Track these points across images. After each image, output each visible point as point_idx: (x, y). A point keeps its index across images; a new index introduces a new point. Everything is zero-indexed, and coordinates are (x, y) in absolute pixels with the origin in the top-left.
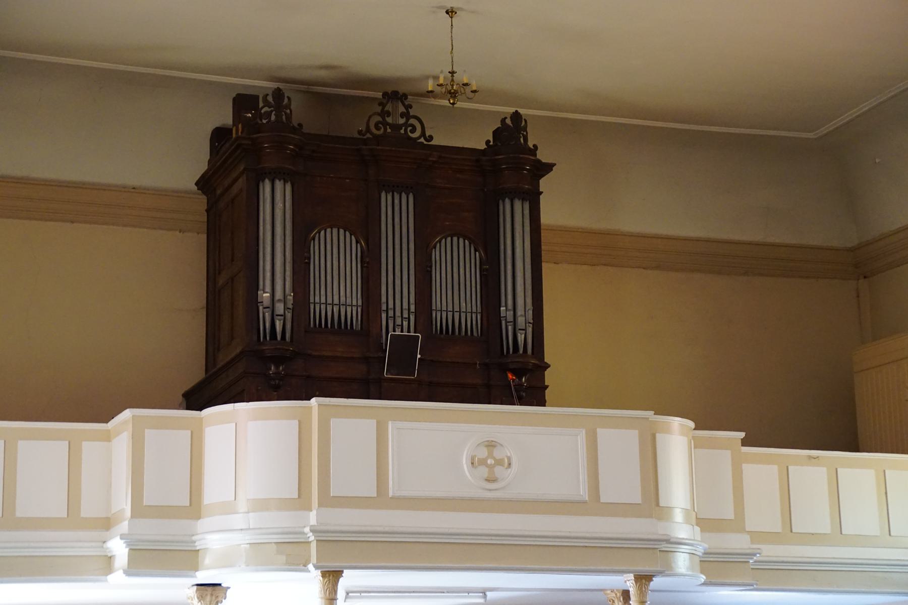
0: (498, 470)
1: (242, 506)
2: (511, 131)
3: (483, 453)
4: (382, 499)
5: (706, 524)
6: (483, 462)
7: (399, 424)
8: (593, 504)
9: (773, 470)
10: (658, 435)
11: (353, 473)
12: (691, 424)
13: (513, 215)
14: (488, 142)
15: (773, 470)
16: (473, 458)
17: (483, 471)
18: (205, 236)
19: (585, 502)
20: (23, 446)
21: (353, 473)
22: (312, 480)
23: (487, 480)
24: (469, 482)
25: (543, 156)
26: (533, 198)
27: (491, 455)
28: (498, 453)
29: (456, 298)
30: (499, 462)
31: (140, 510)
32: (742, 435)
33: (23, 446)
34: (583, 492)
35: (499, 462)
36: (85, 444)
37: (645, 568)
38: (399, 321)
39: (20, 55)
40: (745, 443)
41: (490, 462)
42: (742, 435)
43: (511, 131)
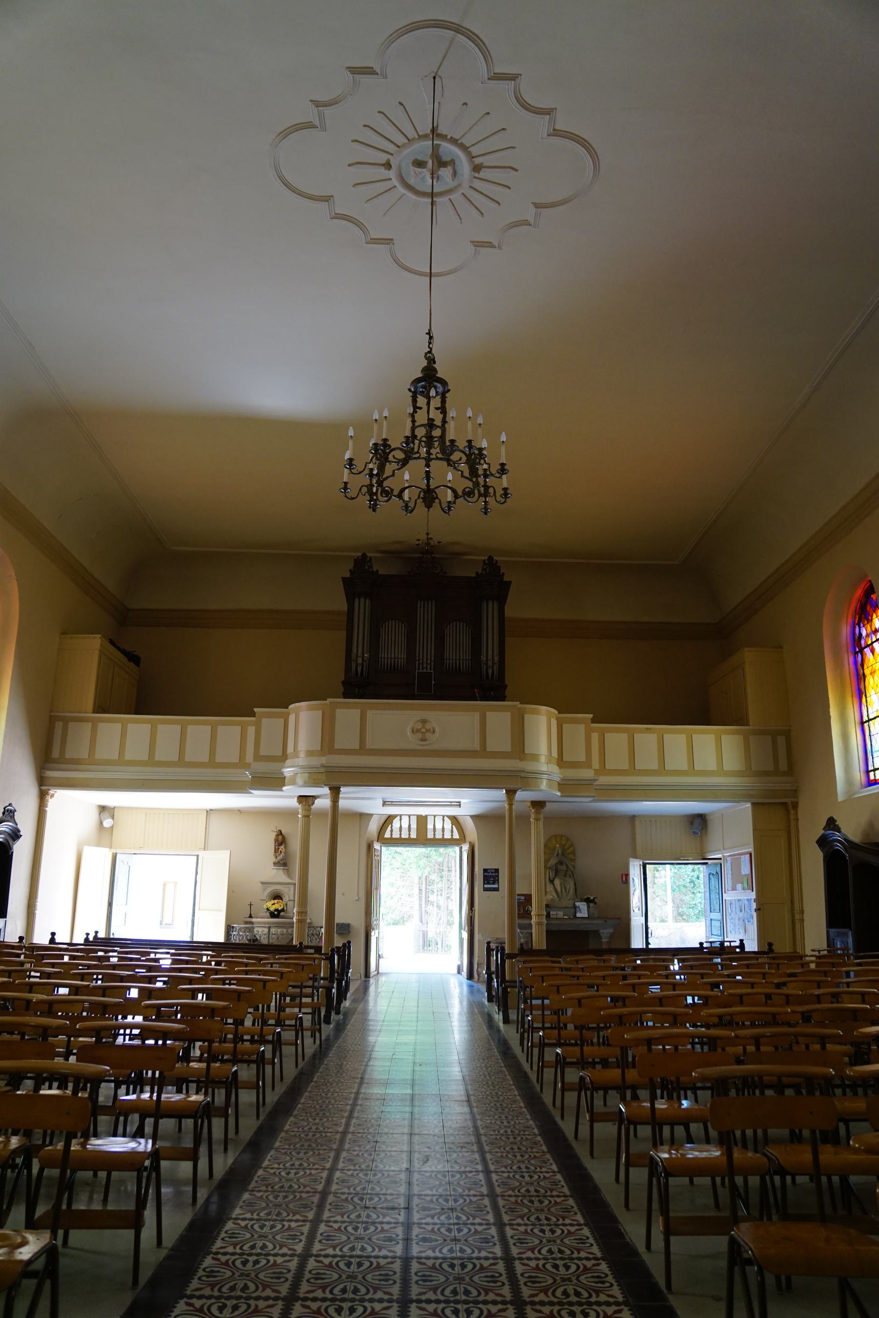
0: (428, 735)
1: (302, 755)
2: (491, 565)
3: (419, 726)
4: (362, 750)
5: (561, 762)
6: (418, 731)
7: (374, 712)
8: (483, 752)
9: (625, 736)
10: (526, 716)
11: (346, 737)
12: (556, 712)
13: (490, 609)
14: (477, 573)
15: (625, 736)
16: (413, 728)
17: (420, 735)
18: (345, 632)
19: (477, 751)
20: (220, 729)
21: (346, 737)
22: (327, 741)
23: (422, 740)
24: (412, 742)
25: (506, 579)
26: (502, 600)
27: (423, 727)
28: (428, 726)
29: (457, 652)
30: (428, 731)
31: (258, 757)
32: (591, 716)
33: (220, 729)
34: (477, 746)
35: (428, 731)
36: (219, 727)
37: (511, 786)
38: (425, 665)
39: (253, 551)
40: (593, 721)
41: (423, 730)
42: (591, 716)
43: (491, 565)
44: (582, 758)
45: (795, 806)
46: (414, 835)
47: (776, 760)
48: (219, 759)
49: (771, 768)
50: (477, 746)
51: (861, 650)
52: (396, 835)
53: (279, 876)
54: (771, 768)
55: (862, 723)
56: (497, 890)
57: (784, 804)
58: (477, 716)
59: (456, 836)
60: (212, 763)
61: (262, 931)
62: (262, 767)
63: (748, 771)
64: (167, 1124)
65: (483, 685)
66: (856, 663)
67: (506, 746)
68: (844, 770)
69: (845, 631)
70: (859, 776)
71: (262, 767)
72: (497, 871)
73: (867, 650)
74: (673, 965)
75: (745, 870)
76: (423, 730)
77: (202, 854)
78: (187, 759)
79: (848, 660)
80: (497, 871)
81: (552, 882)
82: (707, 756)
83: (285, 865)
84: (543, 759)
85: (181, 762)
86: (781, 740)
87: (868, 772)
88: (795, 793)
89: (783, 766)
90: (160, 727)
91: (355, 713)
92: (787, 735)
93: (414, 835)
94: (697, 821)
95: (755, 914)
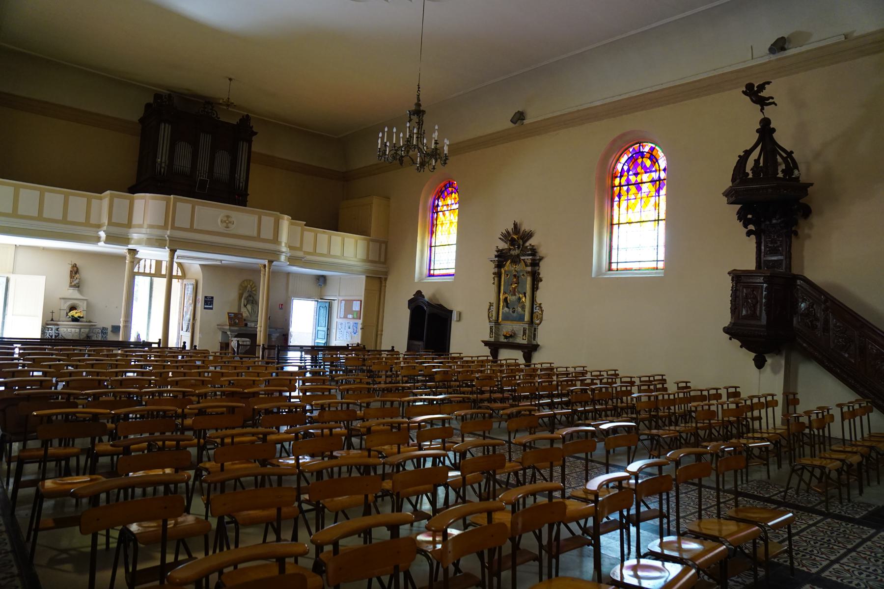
2: (246, 120)
4: (192, 229)
5: (291, 248)
8: (258, 238)
11: (183, 219)
17: (225, 224)
21: (183, 219)
24: (220, 227)
29: (222, 169)
30: (230, 222)
34: (255, 234)
35: (230, 222)
37: (271, 259)
41: (227, 222)
43: (246, 120)
44: (298, 245)
45: (386, 279)
46: (153, 272)
47: (380, 257)
48: (70, 218)
49: (377, 259)
50: (255, 234)
51: (437, 212)
52: (141, 271)
53: (73, 294)
54: (377, 259)
55: (431, 247)
56: (211, 309)
57: (380, 278)
58: (256, 218)
59: (180, 274)
60: (64, 221)
61: (68, 330)
62: (115, 230)
63: (367, 260)
64: (580, 494)
65: (232, 193)
66: (432, 217)
67: (270, 236)
68: (420, 267)
69: (430, 201)
70: (426, 271)
71: (115, 230)
72: (212, 298)
73: (441, 213)
74: (340, 358)
75: (356, 307)
76: (227, 222)
77: (13, 278)
78: (69, 219)
79: (429, 214)
80: (212, 298)
81: (245, 306)
82: (348, 249)
83: (78, 287)
84: (283, 245)
85: (40, 217)
86: (383, 246)
87: (430, 270)
88: (386, 273)
89: (382, 260)
90: (46, 194)
91: (189, 207)
92: (386, 243)
93: (153, 272)
94: (322, 279)
95: (360, 331)
